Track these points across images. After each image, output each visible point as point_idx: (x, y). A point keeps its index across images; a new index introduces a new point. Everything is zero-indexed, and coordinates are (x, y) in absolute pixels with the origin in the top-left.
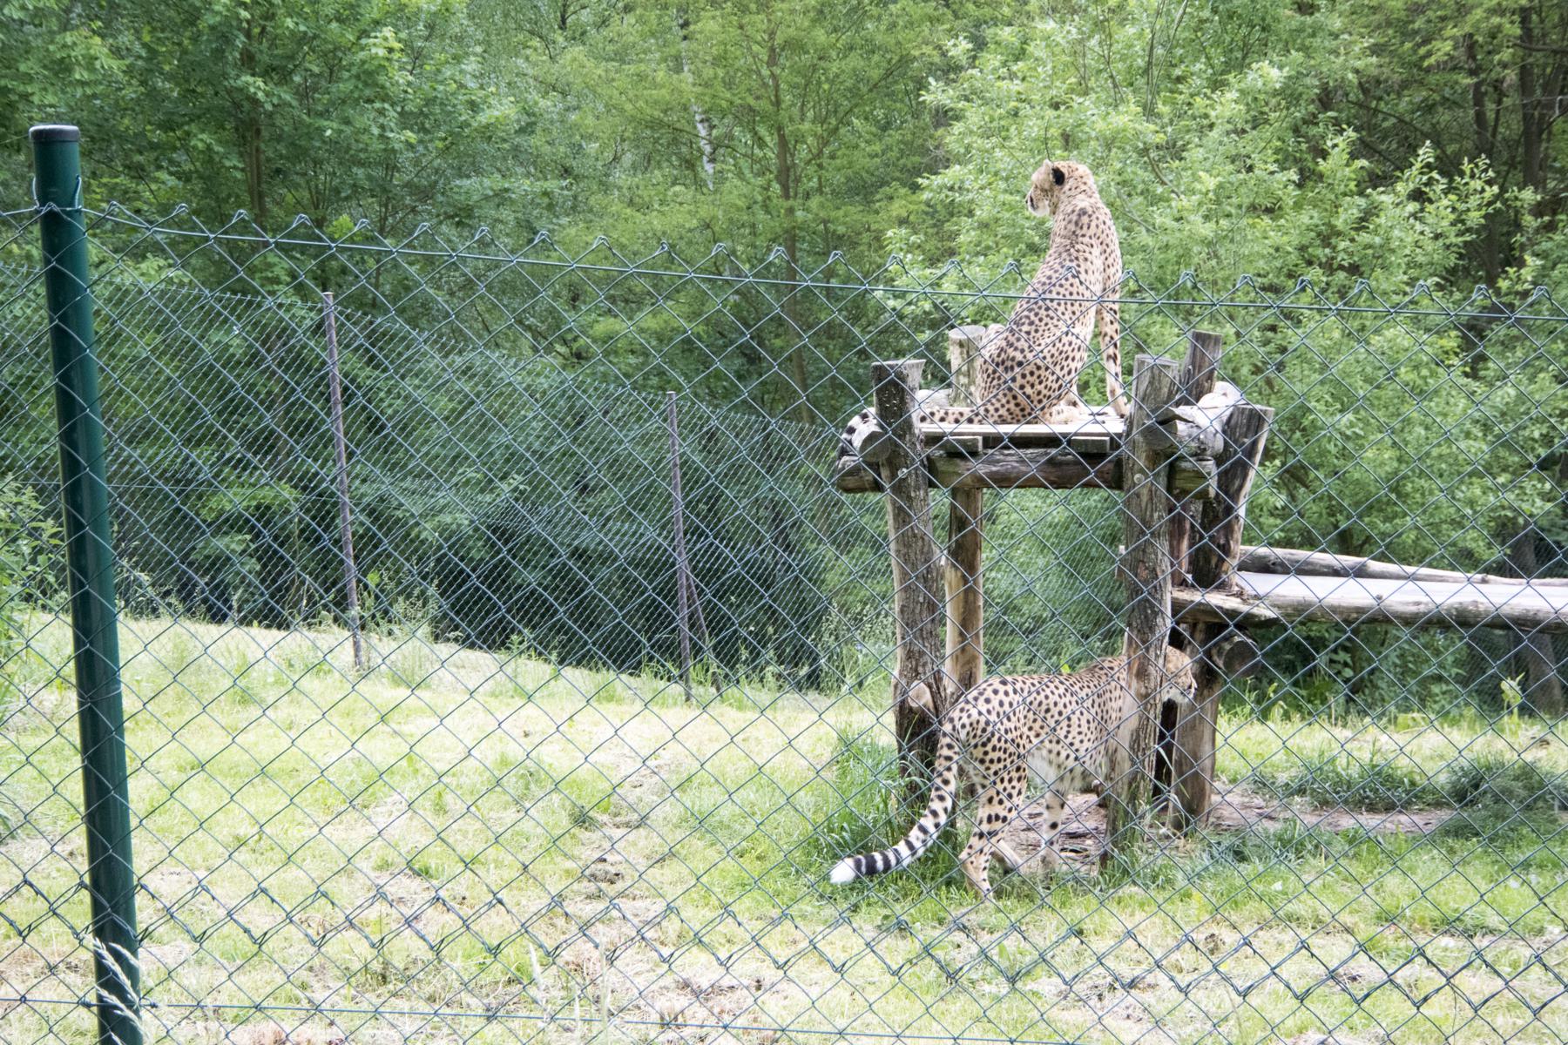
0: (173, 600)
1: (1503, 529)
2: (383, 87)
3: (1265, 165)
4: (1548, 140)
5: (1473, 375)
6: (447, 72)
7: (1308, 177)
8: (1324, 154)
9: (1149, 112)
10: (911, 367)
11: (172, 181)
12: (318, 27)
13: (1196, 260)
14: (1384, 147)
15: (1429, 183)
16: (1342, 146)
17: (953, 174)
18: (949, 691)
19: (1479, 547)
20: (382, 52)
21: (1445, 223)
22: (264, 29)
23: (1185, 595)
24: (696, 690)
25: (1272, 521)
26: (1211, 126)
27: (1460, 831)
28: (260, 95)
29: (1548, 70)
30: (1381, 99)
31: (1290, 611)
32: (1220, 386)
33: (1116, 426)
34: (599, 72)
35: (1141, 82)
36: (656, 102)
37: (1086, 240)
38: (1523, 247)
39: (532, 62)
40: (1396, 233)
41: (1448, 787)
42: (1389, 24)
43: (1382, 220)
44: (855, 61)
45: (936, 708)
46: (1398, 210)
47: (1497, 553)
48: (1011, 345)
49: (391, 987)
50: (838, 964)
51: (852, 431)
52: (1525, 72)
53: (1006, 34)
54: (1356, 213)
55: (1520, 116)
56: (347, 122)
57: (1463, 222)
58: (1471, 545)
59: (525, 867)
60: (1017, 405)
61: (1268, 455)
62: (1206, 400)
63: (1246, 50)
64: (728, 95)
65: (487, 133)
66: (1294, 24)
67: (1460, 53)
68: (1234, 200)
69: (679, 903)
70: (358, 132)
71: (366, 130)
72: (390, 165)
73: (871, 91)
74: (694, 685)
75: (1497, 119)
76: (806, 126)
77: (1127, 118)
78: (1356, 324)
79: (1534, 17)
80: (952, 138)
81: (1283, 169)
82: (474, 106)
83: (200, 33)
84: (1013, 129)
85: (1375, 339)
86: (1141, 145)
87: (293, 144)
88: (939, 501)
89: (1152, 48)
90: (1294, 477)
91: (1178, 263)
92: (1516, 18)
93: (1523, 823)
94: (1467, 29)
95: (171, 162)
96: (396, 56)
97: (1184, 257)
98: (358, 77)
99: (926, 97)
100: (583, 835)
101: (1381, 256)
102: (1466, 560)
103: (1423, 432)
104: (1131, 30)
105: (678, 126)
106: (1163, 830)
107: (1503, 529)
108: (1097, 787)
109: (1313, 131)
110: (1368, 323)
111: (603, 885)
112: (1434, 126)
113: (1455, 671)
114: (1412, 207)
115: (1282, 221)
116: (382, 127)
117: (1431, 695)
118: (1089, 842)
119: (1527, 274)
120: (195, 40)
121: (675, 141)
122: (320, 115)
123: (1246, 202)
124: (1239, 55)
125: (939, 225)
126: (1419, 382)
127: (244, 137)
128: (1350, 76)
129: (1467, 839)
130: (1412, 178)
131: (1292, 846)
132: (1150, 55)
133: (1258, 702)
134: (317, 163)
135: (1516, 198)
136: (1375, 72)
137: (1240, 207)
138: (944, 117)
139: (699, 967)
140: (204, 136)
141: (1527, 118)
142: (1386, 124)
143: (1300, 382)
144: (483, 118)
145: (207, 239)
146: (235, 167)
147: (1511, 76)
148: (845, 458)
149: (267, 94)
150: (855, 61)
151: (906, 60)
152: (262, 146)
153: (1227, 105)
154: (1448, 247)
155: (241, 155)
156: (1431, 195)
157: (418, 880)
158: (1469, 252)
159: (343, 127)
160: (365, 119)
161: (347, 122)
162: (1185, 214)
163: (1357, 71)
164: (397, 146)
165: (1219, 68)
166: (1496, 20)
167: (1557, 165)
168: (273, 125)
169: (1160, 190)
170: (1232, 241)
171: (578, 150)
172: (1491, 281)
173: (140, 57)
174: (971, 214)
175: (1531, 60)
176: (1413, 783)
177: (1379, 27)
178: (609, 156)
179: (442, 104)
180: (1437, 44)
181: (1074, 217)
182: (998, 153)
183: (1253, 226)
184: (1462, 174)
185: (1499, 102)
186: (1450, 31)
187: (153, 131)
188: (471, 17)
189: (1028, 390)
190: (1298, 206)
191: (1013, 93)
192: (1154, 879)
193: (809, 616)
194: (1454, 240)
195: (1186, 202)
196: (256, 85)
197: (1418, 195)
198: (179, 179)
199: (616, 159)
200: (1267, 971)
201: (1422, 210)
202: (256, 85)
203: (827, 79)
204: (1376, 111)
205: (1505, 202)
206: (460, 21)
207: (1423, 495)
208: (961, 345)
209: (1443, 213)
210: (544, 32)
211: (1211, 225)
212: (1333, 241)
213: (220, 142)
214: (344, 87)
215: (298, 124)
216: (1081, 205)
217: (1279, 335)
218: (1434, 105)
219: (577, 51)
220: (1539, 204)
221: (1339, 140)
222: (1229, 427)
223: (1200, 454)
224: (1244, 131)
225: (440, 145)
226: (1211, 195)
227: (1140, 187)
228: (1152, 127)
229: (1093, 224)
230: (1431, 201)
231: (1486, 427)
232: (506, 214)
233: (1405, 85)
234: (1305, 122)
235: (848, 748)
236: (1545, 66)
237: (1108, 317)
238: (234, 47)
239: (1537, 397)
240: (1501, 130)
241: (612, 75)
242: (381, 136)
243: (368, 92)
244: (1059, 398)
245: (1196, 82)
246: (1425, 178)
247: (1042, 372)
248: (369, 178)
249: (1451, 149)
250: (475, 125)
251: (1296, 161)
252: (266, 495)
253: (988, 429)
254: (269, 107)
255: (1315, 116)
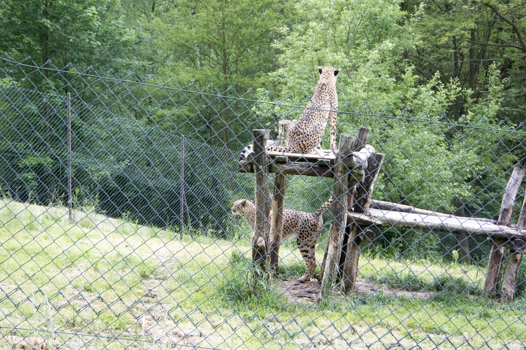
0: (8, 193)
1: (456, 202)
2: (91, 26)
3: (385, 76)
4: (478, 74)
5: (449, 149)
6: (113, 22)
7: (399, 79)
8: (404, 73)
9: (347, 53)
10: (266, 133)
11: (17, 52)
12: (70, 4)
13: (360, 105)
14: (424, 72)
15: (439, 84)
16: (410, 70)
17: (281, 71)
18: (271, 241)
19: (447, 206)
20: (91, 15)
21: (443, 98)
22: (51, 3)
23: (352, 215)
24: (184, 236)
25: (379, 193)
26: (368, 60)
27: (437, 299)
28: (49, 26)
29: (479, 51)
30: (423, 56)
31: (386, 222)
32: (367, 146)
33: (332, 156)
34: (165, 27)
35: (345, 44)
36: (183, 38)
37: (324, 93)
38: (467, 108)
39: (142, 21)
40: (426, 100)
41: (433, 284)
42: (428, 32)
43: (422, 96)
44: (251, 30)
45: (266, 246)
46: (427, 93)
47: (453, 208)
48: (300, 127)
49: (76, 328)
50: (233, 328)
51: (244, 152)
52: (471, 51)
53: (300, 27)
54: (414, 93)
55: (469, 65)
56: (78, 37)
57: (449, 98)
58: (443, 205)
59: (130, 288)
60: (300, 147)
61: (381, 171)
62: (363, 150)
63: (380, 36)
64: (208, 38)
65: (125, 44)
66: (396, 29)
67: (451, 43)
68: (374, 86)
69: (181, 304)
70: (81, 40)
71: (84, 40)
72: (92, 53)
73: (255, 40)
74: (184, 234)
75: (461, 66)
76: (233, 50)
77: (340, 57)
78: (411, 130)
79: (476, 33)
80: (281, 58)
81: (391, 77)
82: (121, 34)
83: (29, 3)
84: (301, 57)
85: (417, 135)
86: (343, 66)
87: (59, 43)
88: (271, 178)
89: (349, 33)
90: (387, 180)
91: (354, 105)
92: (470, 32)
93: (457, 298)
94: (454, 34)
95: (16, 45)
96: (95, 16)
97: (356, 103)
98: (82, 22)
99: (273, 45)
100: (144, 281)
101: (420, 108)
102: (443, 210)
103: (431, 167)
104: (342, 27)
105: (190, 47)
106: (339, 292)
107: (456, 202)
108: (318, 276)
109: (401, 64)
110: (415, 130)
111: (150, 298)
112: (440, 66)
113: (436, 247)
114: (432, 92)
115: (390, 95)
116: (90, 39)
117: (427, 254)
118: (314, 295)
119: (469, 117)
120: (28, 5)
121: (188, 52)
122: (69, 34)
123: (378, 87)
124: (378, 38)
125: (275, 86)
126: (431, 150)
127: (42, 39)
128: (414, 47)
129: (439, 302)
130: (432, 82)
131: (382, 300)
132: (348, 36)
133: (372, 252)
134: (67, 50)
135: (466, 92)
136: (422, 46)
137: (376, 88)
138: (279, 52)
139: (186, 328)
140: (28, 38)
141: (471, 66)
142: (425, 64)
143: (391, 147)
144: (124, 38)
145: (36, 68)
146: (38, 49)
147: (466, 51)
148: (242, 161)
149: (51, 25)
150: (251, 30)
151: (268, 31)
152: (48, 43)
153: (374, 54)
154: (443, 107)
155: (41, 45)
156: (439, 89)
157: (87, 292)
158: (450, 108)
159: (76, 39)
160: (84, 36)
161: (78, 37)
162: (357, 89)
163: (417, 46)
164: (94, 46)
165: (370, 42)
166: (463, 32)
167: (479, 82)
168: (52, 36)
169: (350, 80)
170: (372, 99)
171: (155, 52)
172: (456, 119)
173: (9, 9)
174: (286, 84)
175: (474, 47)
176: (422, 282)
177: (425, 32)
178: (165, 55)
179: (110, 33)
180: (443, 38)
181: (321, 86)
182: (296, 65)
183: (380, 95)
184: (450, 83)
185: (463, 60)
186: (448, 34)
187: (11, 35)
188: (122, 5)
189: (304, 142)
190: (395, 89)
191: (302, 46)
192: (335, 308)
193: (221, 214)
194: (445, 104)
195: (357, 85)
196: (47, 22)
197: (434, 88)
198: (19, 51)
199: (168, 56)
200: (377, 339)
201: (436, 93)
202: (47, 22)
203: (241, 35)
204: (422, 60)
205: (462, 93)
206: (118, 5)
207: (429, 188)
208: (283, 126)
209: (443, 95)
210: (146, 12)
211: (365, 94)
212: (405, 101)
213: (34, 40)
214: (78, 25)
215: (61, 36)
216: (324, 82)
217: (386, 131)
218: (441, 59)
219: (158, 19)
220: (473, 94)
221: (409, 68)
222: (370, 160)
223: (360, 168)
224: (379, 63)
225: (109, 46)
226: (366, 84)
227: (343, 79)
228: (347, 60)
229: (327, 89)
230: (439, 91)
231: (451, 167)
232: (130, 73)
233: (432, 52)
234: (398, 61)
235: (236, 258)
236: (478, 49)
237: (333, 120)
238: (41, 9)
239: (469, 158)
240: (463, 69)
241: (169, 28)
242: (89, 42)
243: (86, 28)
244: (315, 146)
245: (363, 46)
246: (436, 83)
247: (309, 137)
248: (84, 56)
249: (446, 74)
250: (121, 41)
251: (395, 74)
252: (42, 160)
253: (290, 154)
254: (51, 30)
255: (402, 60)
